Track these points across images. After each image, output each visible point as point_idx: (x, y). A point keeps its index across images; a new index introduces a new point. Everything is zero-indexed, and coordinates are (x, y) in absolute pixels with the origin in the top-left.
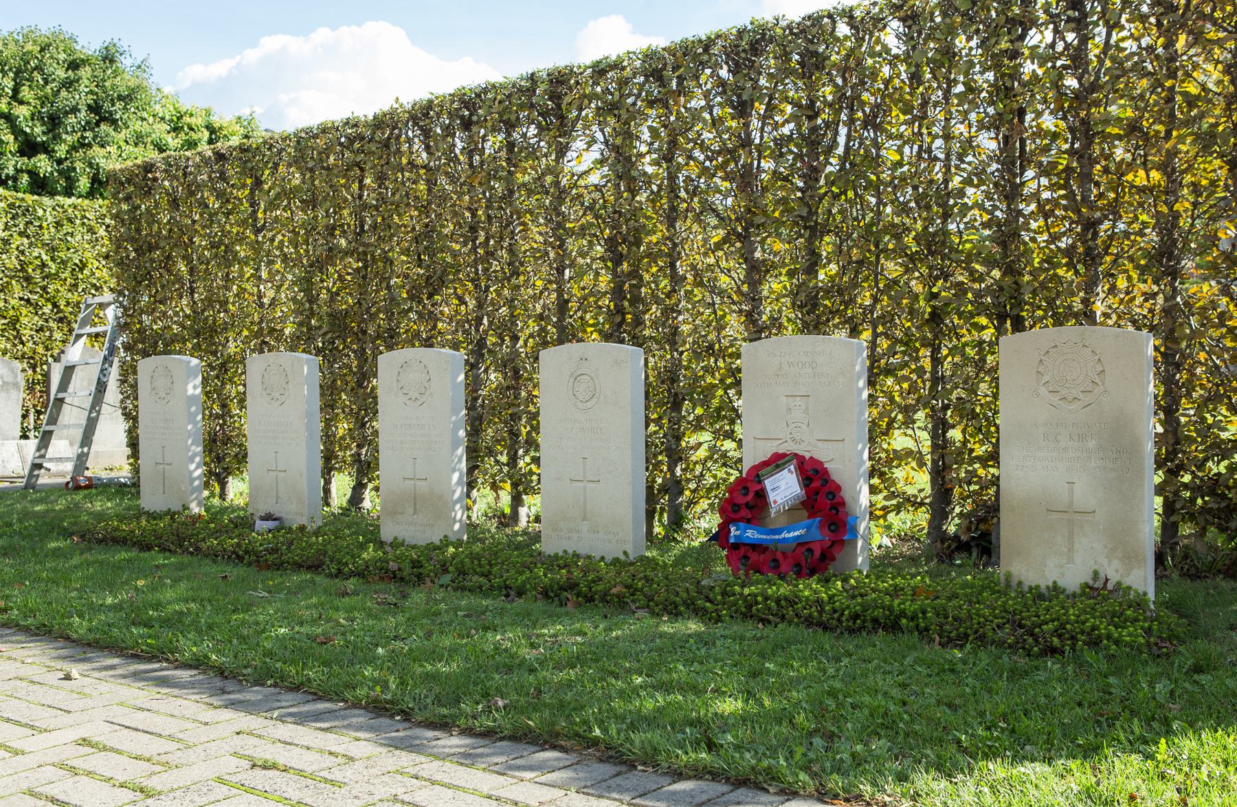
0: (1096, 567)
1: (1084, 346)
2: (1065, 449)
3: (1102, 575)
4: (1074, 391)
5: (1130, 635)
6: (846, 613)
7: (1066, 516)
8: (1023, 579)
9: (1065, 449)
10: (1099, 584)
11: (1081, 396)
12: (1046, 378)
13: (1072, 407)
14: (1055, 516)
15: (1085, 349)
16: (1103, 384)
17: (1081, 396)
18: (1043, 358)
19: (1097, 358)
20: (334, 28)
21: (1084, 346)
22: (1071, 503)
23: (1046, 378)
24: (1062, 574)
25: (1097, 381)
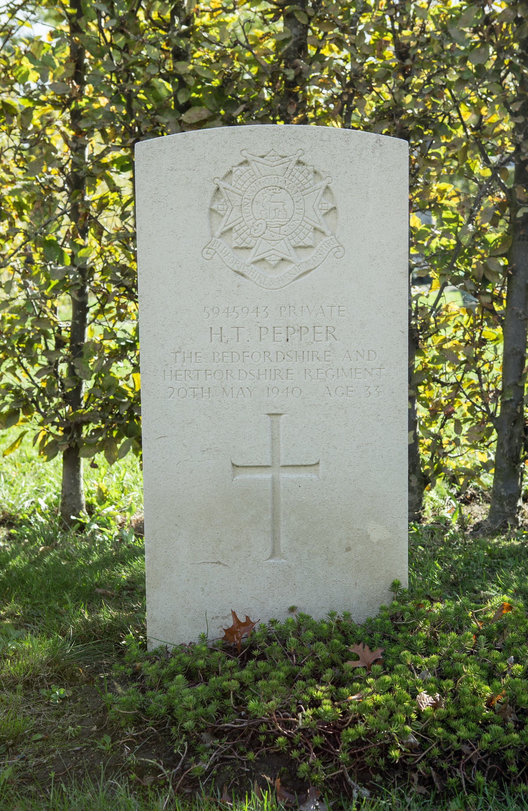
11: (293, 255)
17: (293, 255)
19: (322, 184)
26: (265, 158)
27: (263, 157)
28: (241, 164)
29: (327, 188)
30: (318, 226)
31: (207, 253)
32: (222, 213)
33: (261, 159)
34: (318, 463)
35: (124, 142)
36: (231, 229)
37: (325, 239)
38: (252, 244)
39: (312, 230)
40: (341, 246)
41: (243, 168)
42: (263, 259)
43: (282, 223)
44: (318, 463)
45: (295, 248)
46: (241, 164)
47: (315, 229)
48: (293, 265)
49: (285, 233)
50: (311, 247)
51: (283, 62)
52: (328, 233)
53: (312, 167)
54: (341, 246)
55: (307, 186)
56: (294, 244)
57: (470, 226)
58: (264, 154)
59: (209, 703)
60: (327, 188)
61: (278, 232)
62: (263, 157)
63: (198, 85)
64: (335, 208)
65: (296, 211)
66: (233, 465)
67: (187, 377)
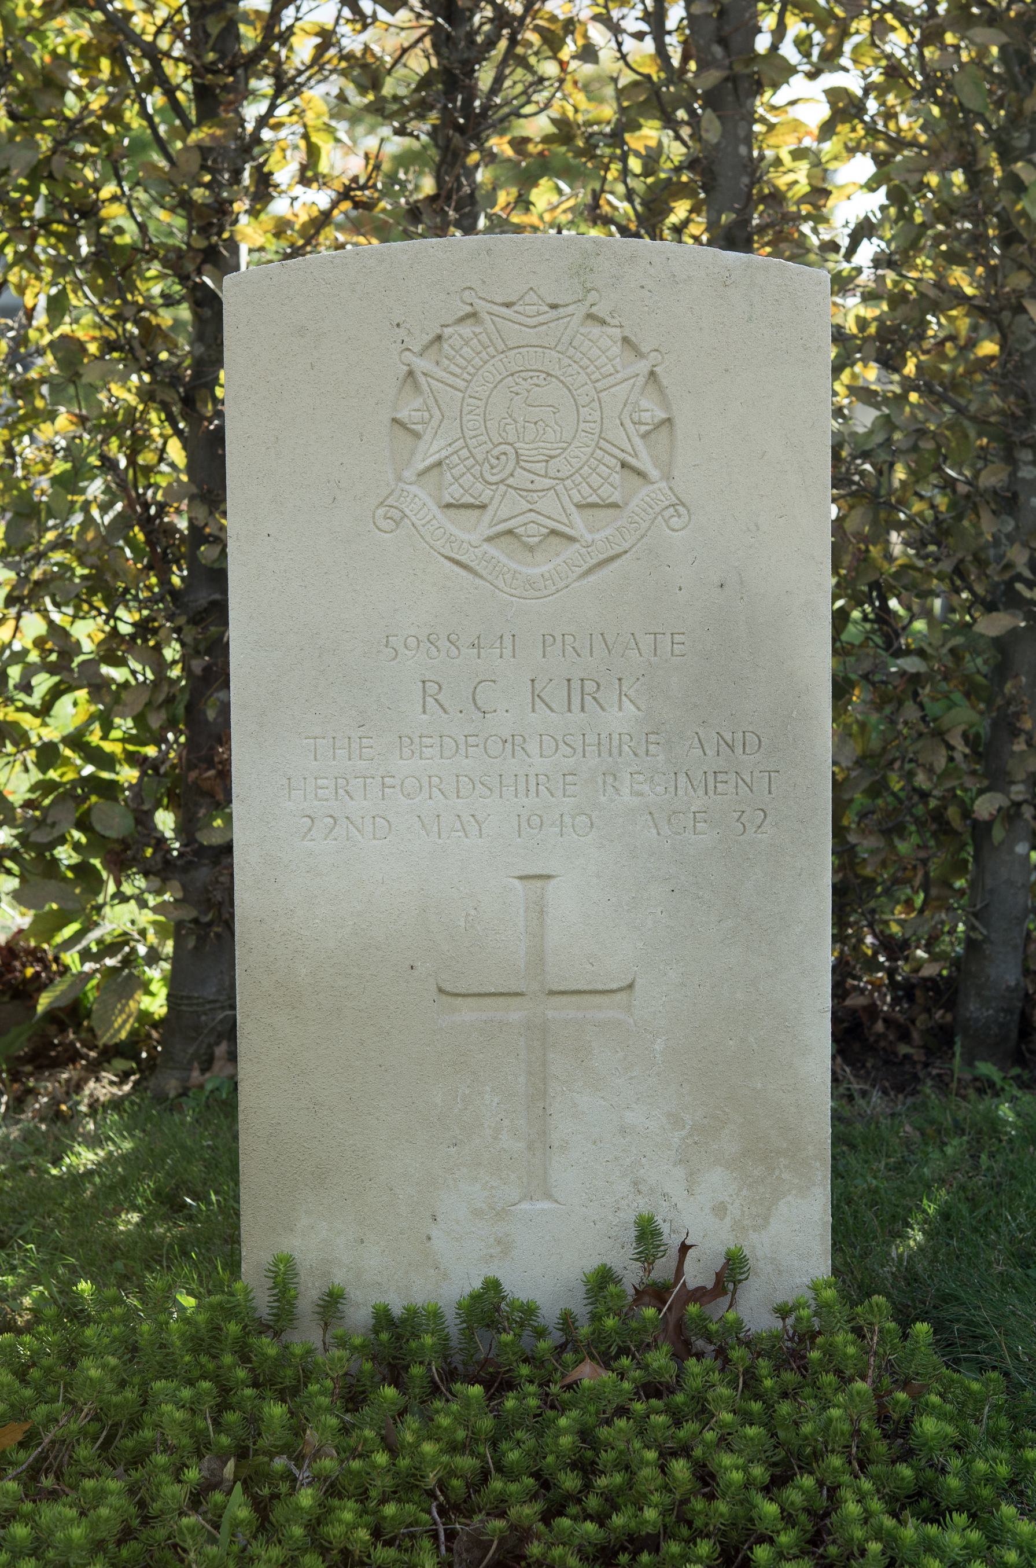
0: (642, 1205)
1: (590, 316)
2: (513, 743)
3: (673, 1242)
4: (548, 504)
5: (101, 1495)
6: (865, 1426)
7: (515, 1013)
8: (339, 1278)
9: (513, 743)
10: (663, 1269)
11: (578, 524)
12: (431, 450)
13: (539, 568)
14: (468, 1013)
15: (596, 330)
16: (668, 477)
17: (578, 524)
18: (421, 364)
19: (642, 367)
20: (759, 30)
21: (590, 316)
22: (538, 959)
23: (431, 450)
24: (505, 1245)
25: (644, 462)
26: (516, 308)
27: (508, 305)
28: (461, 320)
29: (652, 373)
30: (633, 461)
31: (386, 518)
32: (418, 428)
33: (504, 310)
34: (631, 986)
35: (85, 601)
36: (439, 464)
37: (646, 490)
38: (485, 499)
39: (618, 468)
40: (683, 505)
41: (466, 330)
42: (510, 532)
43: (553, 453)
44: (631, 986)
45: (579, 506)
46: (461, 320)
47: (624, 465)
48: (577, 545)
49: (559, 475)
50: (615, 505)
51: (478, 111)
52: (654, 473)
53: (619, 330)
54: (683, 505)
55: (609, 369)
56: (577, 498)
57: (897, 436)
58: (513, 299)
59: (388, 1543)
60: (652, 373)
61: (543, 472)
62: (508, 305)
63: (973, 15)
64: (669, 420)
65: (582, 426)
66: (441, 990)
67: (341, 791)
